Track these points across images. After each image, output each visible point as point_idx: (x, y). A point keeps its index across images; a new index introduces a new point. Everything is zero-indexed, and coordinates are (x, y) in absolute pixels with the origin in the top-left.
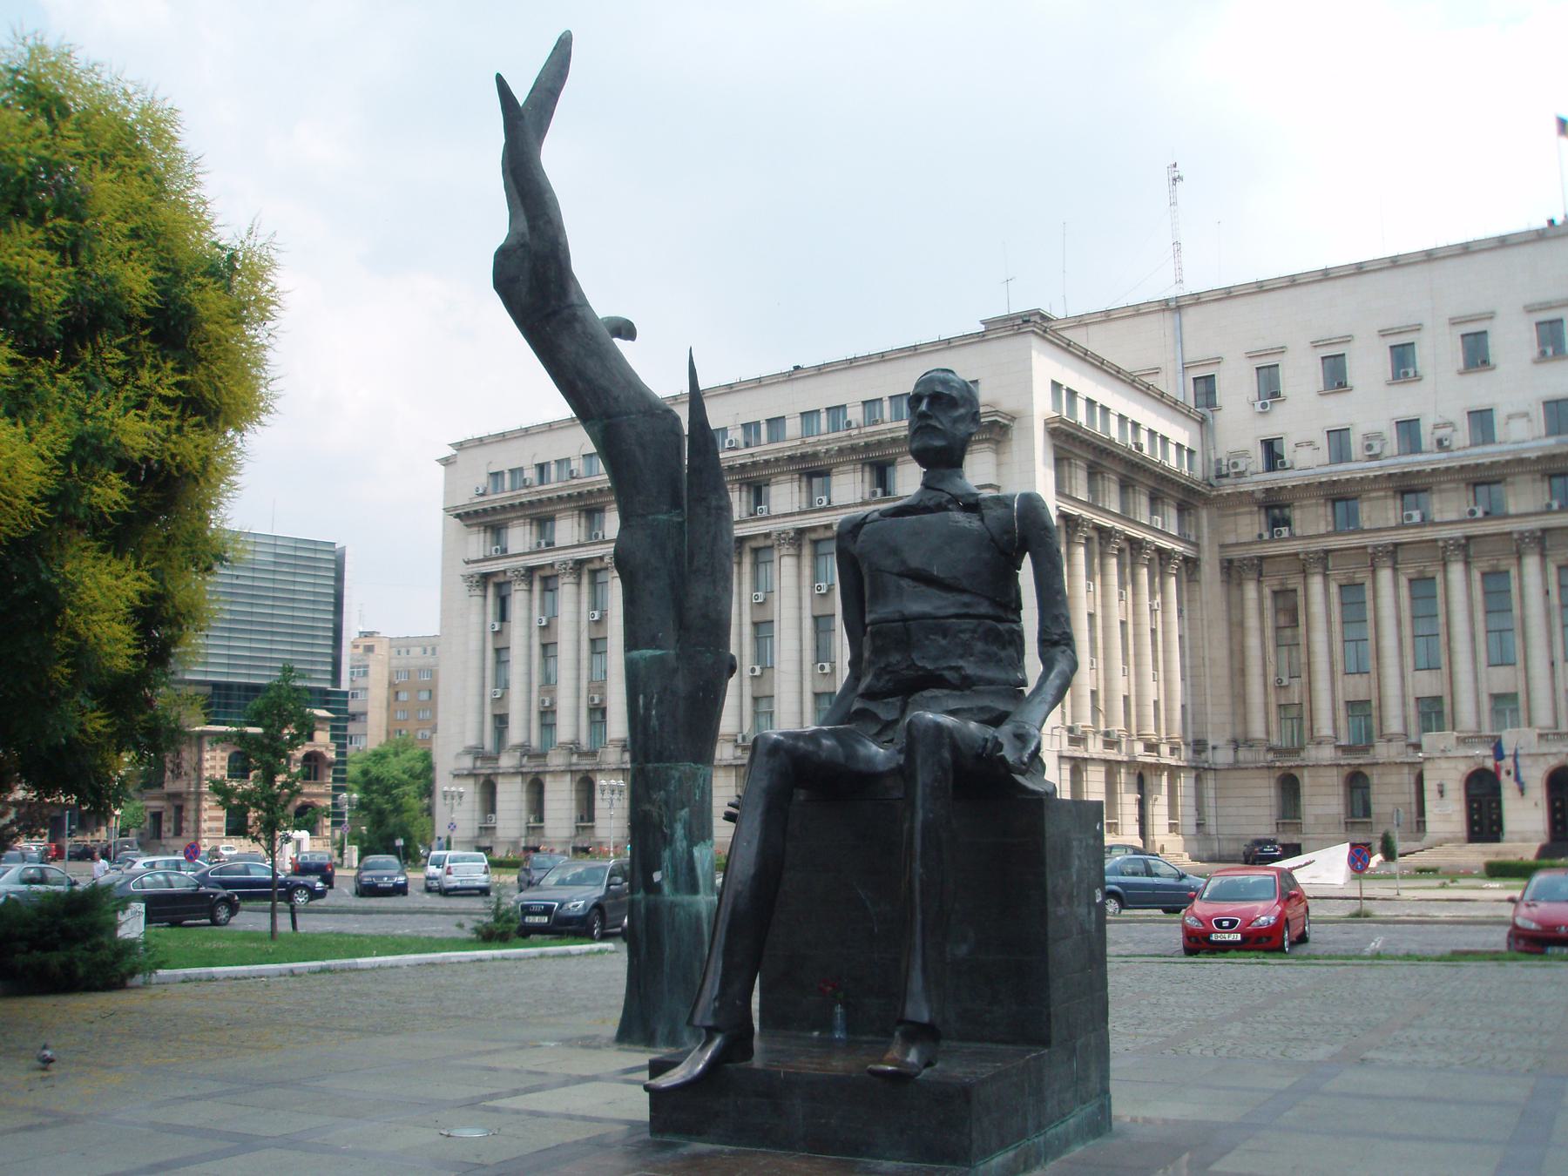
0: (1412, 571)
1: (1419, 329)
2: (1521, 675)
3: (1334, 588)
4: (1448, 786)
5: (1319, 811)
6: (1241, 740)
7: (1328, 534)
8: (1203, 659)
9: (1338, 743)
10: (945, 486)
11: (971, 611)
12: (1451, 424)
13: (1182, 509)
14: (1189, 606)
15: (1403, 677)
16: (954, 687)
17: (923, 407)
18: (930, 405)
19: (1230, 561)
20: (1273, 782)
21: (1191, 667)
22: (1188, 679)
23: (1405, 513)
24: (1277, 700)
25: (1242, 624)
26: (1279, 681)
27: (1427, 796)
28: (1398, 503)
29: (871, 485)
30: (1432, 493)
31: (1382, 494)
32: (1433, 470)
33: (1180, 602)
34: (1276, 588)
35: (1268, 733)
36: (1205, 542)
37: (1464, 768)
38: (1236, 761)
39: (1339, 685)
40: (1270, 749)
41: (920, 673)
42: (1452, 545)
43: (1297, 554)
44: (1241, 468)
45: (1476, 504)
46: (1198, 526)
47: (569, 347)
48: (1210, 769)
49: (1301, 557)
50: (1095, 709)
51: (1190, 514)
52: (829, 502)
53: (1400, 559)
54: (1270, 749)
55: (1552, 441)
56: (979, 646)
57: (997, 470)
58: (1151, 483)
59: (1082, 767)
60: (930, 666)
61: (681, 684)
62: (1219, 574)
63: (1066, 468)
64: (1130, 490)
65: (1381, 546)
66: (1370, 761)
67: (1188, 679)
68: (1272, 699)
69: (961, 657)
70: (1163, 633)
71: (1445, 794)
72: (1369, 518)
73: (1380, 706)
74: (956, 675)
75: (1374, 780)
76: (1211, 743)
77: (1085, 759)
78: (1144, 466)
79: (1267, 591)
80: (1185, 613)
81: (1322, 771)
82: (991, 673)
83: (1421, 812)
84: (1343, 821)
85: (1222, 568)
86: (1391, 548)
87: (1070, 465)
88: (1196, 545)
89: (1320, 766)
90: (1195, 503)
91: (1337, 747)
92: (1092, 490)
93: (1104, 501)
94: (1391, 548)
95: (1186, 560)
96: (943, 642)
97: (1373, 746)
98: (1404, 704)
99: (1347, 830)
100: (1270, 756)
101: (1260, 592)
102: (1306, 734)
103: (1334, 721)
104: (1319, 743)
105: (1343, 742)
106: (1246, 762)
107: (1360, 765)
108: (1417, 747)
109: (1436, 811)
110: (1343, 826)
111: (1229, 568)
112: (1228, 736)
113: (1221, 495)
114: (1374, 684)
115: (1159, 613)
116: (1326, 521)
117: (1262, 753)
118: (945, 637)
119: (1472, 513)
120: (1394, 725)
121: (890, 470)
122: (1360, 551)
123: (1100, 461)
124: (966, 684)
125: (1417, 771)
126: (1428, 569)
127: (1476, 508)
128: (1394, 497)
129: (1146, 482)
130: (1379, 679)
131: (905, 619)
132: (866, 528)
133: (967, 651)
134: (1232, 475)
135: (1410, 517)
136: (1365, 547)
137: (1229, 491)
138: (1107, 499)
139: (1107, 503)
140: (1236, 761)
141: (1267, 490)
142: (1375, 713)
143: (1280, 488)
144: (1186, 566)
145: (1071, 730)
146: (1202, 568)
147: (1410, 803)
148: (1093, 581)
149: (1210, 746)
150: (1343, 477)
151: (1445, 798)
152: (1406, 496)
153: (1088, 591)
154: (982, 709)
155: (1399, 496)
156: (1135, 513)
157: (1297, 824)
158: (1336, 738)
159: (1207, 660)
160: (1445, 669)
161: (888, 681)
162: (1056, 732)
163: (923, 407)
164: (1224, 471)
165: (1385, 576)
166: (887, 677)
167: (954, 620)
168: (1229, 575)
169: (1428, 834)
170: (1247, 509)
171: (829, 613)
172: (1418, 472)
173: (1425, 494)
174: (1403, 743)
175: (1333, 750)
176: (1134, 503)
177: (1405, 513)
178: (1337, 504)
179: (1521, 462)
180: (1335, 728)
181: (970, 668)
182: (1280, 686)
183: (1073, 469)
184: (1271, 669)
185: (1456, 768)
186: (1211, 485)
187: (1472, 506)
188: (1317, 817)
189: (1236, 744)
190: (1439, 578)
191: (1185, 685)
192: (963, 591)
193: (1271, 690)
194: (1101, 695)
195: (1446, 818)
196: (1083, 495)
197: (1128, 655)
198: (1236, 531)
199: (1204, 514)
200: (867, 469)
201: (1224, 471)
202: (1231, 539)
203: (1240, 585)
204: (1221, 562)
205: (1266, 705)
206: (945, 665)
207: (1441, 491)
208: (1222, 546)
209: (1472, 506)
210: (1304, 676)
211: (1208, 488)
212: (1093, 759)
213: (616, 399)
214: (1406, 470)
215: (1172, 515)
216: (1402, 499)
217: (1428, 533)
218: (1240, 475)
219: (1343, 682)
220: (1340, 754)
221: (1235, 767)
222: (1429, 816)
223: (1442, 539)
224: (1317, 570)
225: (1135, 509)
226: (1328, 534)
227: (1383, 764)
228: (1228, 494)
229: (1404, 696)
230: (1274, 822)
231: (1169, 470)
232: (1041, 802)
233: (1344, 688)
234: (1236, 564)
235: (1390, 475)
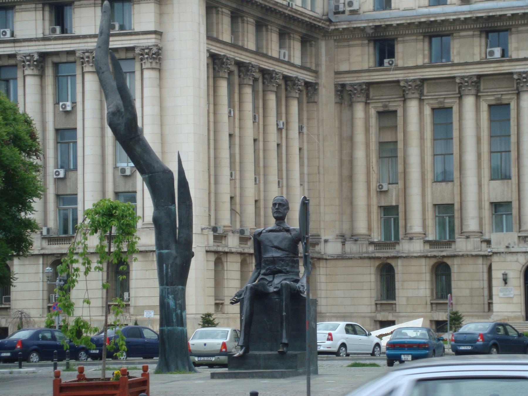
0: (491, 99)
3: (427, 111)
4: (511, 275)
5: (410, 294)
6: (348, 234)
7: (423, 67)
8: (319, 167)
9: (427, 239)
10: (282, 225)
11: (289, 256)
13: (305, 41)
14: (308, 123)
15: (480, 186)
16: (285, 273)
17: (277, 207)
18: (278, 206)
19: (343, 86)
20: (373, 270)
21: (309, 174)
22: (306, 185)
23: (488, 50)
24: (379, 203)
25: (351, 139)
26: (380, 187)
27: (494, 282)
28: (483, 41)
29: (51, 24)
31: (471, 33)
32: (513, 15)
33: (300, 120)
34: (381, 109)
35: (370, 229)
36: (323, 69)
38: (344, 252)
39: (429, 191)
40: (371, 243)
42: (524, 78)
43: (398, 82)
44: (355, 7)
46: (318, 56)
47: (138, 150)
48: (323, 259)
49: (402, 84)
50: (233, 210)
51: (311, 45)
52: (12, 35)
53: (482, 88)
54: (371, 243)
56: (290, 264)
57: (160, 19)
58: (280, 22)
59: (224, 259)
60: (280, 269)
61: (178, 261)
62: (334, 97)
63: (215, 15)
64: (264, 29)
65: (467, 77)
66: (452, 254)
67: (306, 185)
68: (374, 201)
69: (286, 266)
70: (287, 147)
71: (508, 281)
72: (459, 53)
73: (461, 209)
75: (455, 269)
76: (323, 238)
77: (226, 253)
78: (275, 10)
79: (373, 112)
80: (305, 130)
81: (414, 262)
82: (293, 270)
83: (490, 296)
84: (429, 303)
85: (337, 91)
86: (475, 79)
87: (217, 13)
88: (316, 72)
89: (412, 257)
90: (315, 36)
91: (426, 242)
92: (234, 32)
93: (243, 40)
94: (475, 79)
95: (307, 84)
96: (283, 263)
97: (454, 242)
98: (480, 208)
99: (432, 310)
100: (371, 248)
101: (367, 112)
102: (401, 231)
103: (424, 220)
104: (411, 239)
105: (431, 237)
106: (351, 253)
107: (444, 257)
108: (488, 242)
109: (501, 295)
110: (429, 306)
111: (341, 92)
112: (337, 232)
113: (337, 30)
114: (457, 191)
115: (284, 131)
116: (424, 55)
117: (365, 246)
118: (283, 262)
120: (472, 225)
121: (67, 9)
122: (451, 80)
123: (241, 8)
124: (287, 272)
125: (489, 263)
126: (503, 97)
128: (480, 36)
129: (276, 22)
130: (461, 186)
131: (274, 257)
132: (262, 234)
133: (288, 265)
134: (347, 13)
135: (492, 53)
136: (454, 78)
137: (345, 26)
138: (246, 39)
139: (246, 43)
140: (344, 252)
141: (377, 27)
142: (457, 214)
143: (387, 26)
144: (307, 89)
145: (215, 229)
146: (320, 91)
147: (483, 288)
148: (234, 108)
149: (322, 240)
150: (439, 19)
152: (490, 35)
153: (229, 116)
154: (292, 278)
155: (484, 35)
156: (267, 48)
157: (392, 304)
158: (425, 234)
159: (321, 168)
160: (514, 179)
162: (205, 232)
163: (277, 207)
164: (341, 8)
165: (469, 101)
168: (342, 98)
170: (359, 42)
171: (131, 190)
172: (501, 16)
173: (505, 33)
174: (479, 239)
175: (422, 244)
176: (267, 40)
177: (488, 50)
178: (434, 39)
180: (424, 226)
181: (288, 269)
182: (382, 192)
183: (220, 16)
184: (374, 177)
185: (517, 261)
186: (330, 21)
188: (408, 298)
189: (343, 238)
190: (513, 105)
191: (304, 190)
193: (373, 194)
194: (238, 199)
195: (509, 300)
196: (226, 37)
197: (259, 166)
198: (349, 60)
199: (323, 45)
200: (47, 8)
201: (341, 8)
202: (344, 67)
203: (351, 105)
204: (336, 85)
205: (369, 206)
207: (518, 32)
208: (337, 73)
210: (401, 183)
211: (328, 23)
212: (232, 253)
213: (154, 167)
214: (491, 14)
215: (296, 46)
216: (487, 37)
217: (506, 68)
218: (354, 12)
219: (432, 187)
220: (427, 247)
221: (341, 257)
222: (495, 299)
223: (516, 73)
224: (414, 96)
225: (267, 45)
226: (423, 67)
227: (463, 256)
228: (344, 29)
229: (480, 201)
230: (373, 303)
231: (296, 11)
232: (304, 299)
233: (433, 194)
234: (348, 88)
235: (478, 18)
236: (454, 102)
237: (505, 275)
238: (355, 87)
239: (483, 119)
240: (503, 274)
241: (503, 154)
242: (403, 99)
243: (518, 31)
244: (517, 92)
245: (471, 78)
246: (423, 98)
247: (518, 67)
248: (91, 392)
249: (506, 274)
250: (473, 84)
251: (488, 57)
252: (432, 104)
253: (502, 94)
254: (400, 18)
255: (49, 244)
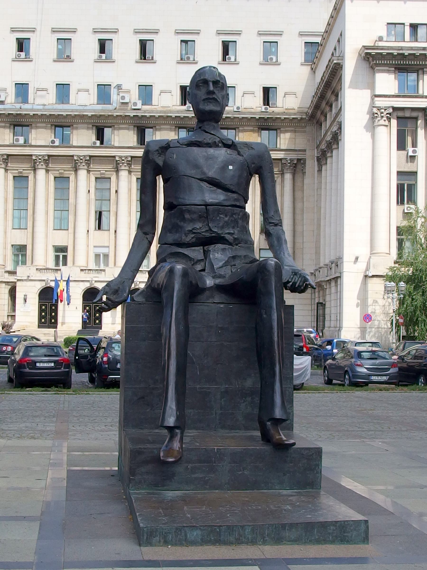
0: (57, 174)
1: (34, 31)
2: (71, 236)
12: (46, 90)
30: (32, 128)
37: (40, 286)
41: (213, 235)
45: (55, 138)
55: (100, 107)
71: (27, 301)
74: (231, 238)
119: (53, 142)
127: (55, 140)
135: (17, 140)
151: (27, 303)
160: (71, 230)
161: (193, 238)
166: (193, 235)
167: (230, 208)
169: (16, 323)
179: (83, 117)
187: (53, 138)
192: (233, 192)
206: (227, 232)
209: (53, 138)
217: (27, 151)
223: (35, 155)
236: (71, 174)
237: (25, 296)
238: (40, 157)
239: (9, 186)
240: (24, 295)
241: (22, 211)
242: (116, 170)
243: (36, 127)
244: (34, 168)
245: (85, 157)
246: (7, 168)
247: (36, 151)
248: (277, 393)
249: (26, 295)
250: (4, 160)
251: (15, 143)
252: (54, 174)
253: (23, 169)
254: (77, 110)
255: (292, 272)
